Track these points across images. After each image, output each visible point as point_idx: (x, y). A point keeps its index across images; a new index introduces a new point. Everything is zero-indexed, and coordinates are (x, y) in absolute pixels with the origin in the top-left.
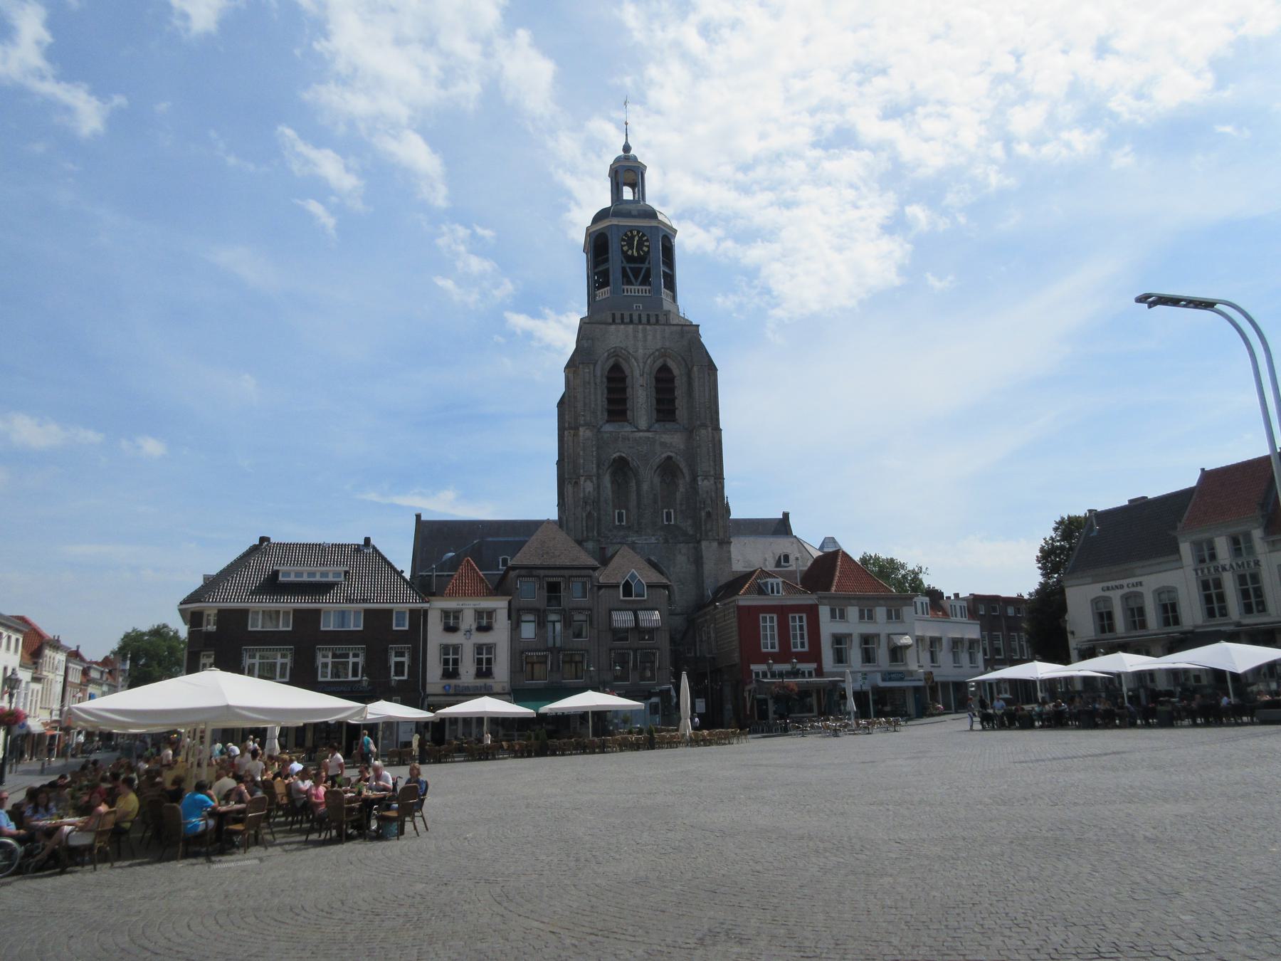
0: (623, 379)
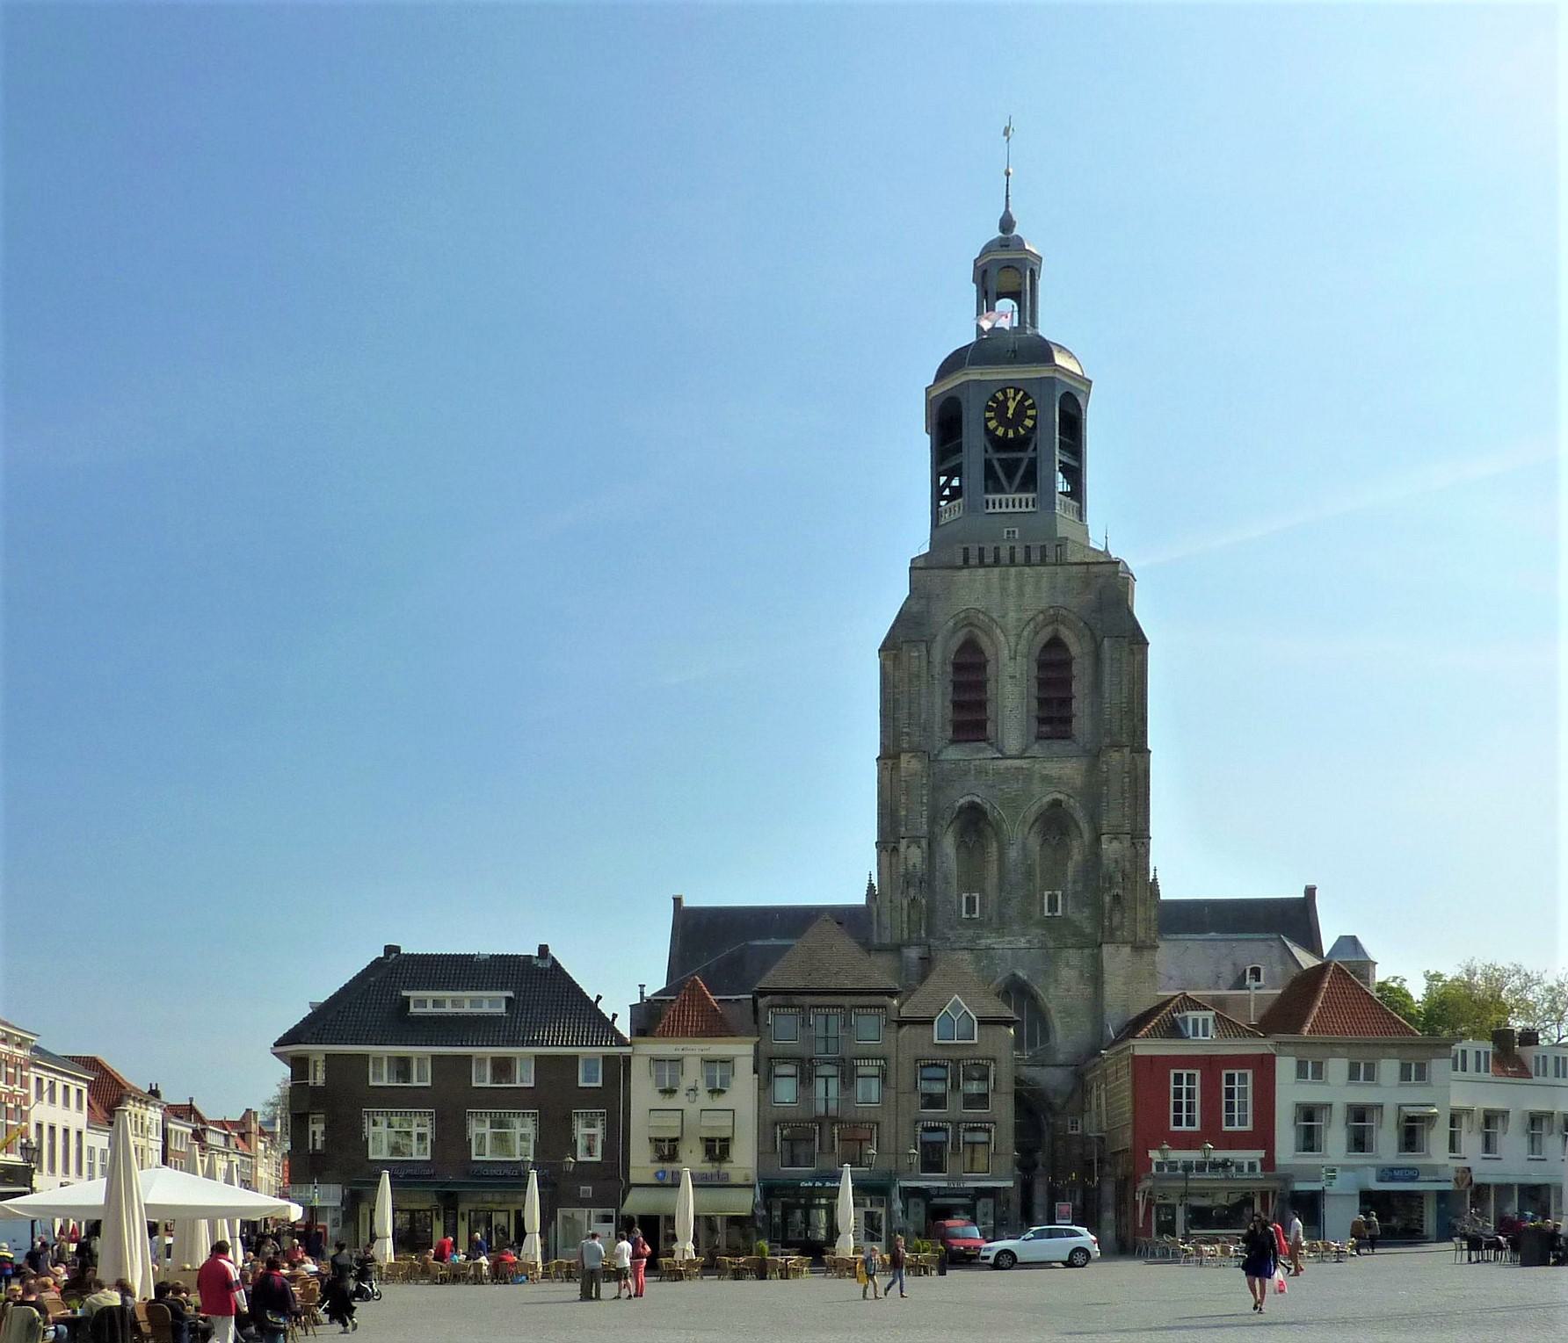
0: (981, 666)
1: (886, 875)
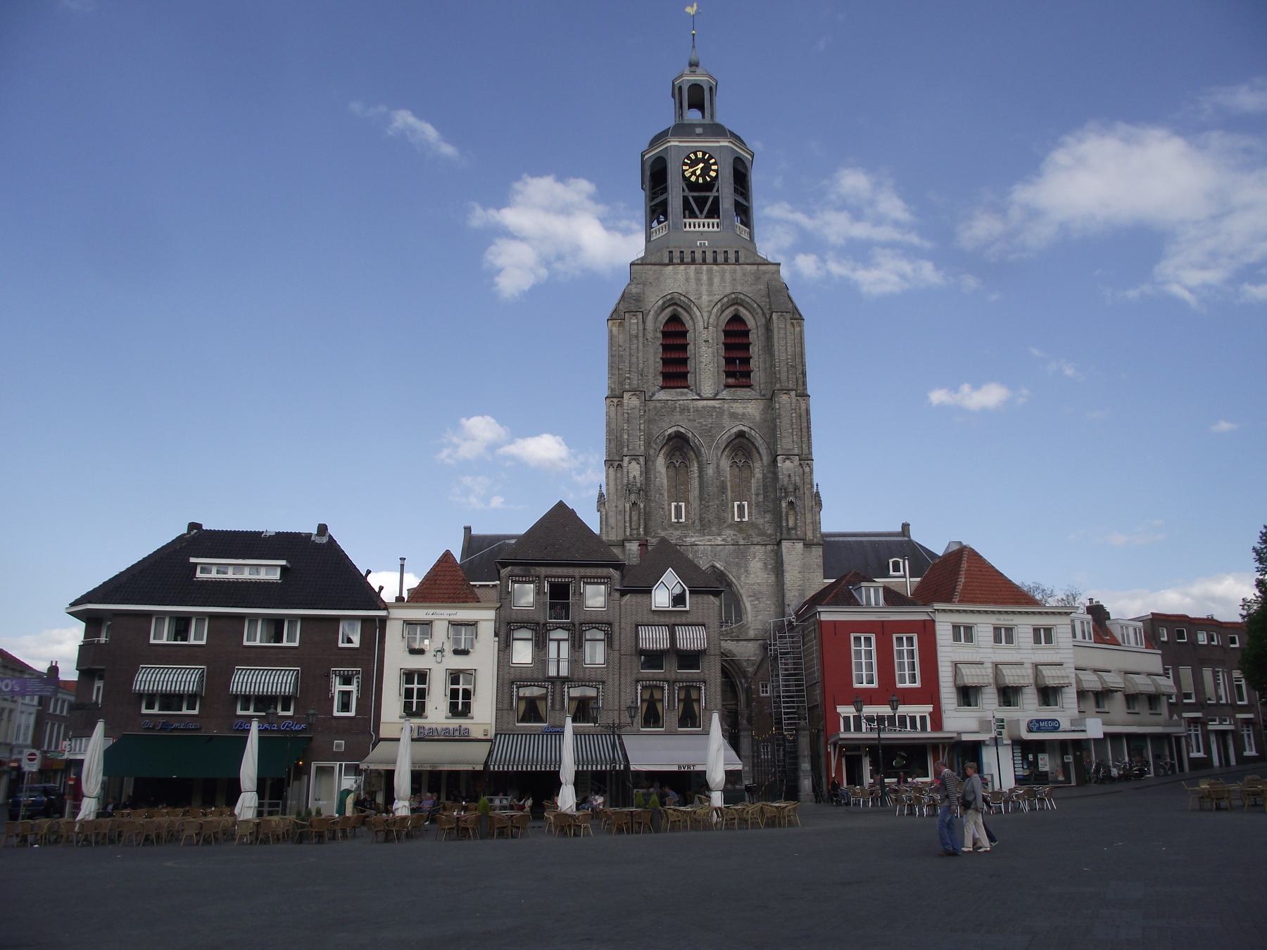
1: (612, 483)
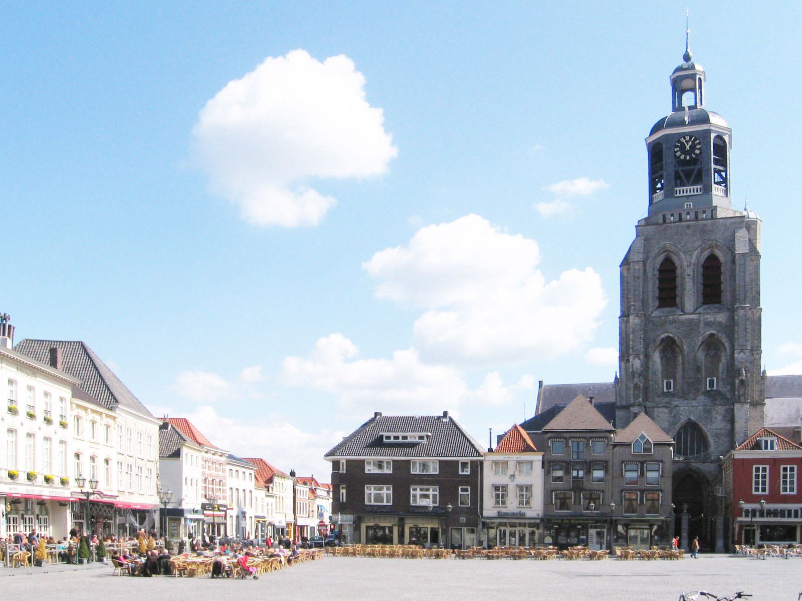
0: (674, 270)
1: (623, 372)
